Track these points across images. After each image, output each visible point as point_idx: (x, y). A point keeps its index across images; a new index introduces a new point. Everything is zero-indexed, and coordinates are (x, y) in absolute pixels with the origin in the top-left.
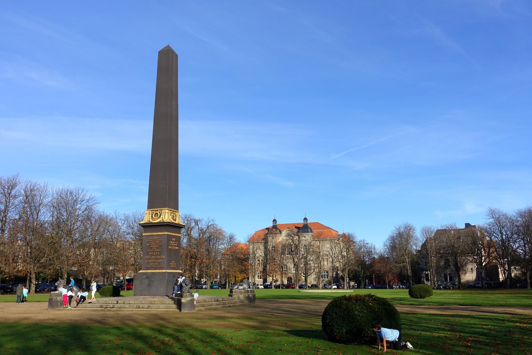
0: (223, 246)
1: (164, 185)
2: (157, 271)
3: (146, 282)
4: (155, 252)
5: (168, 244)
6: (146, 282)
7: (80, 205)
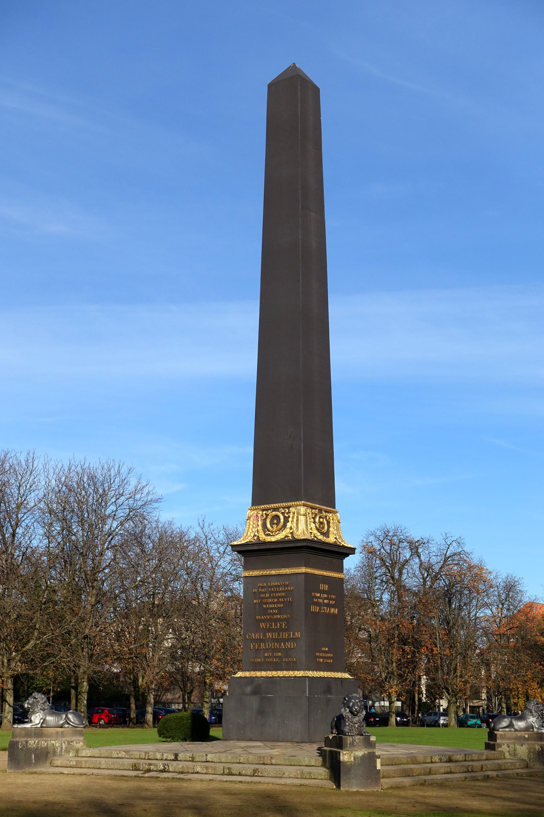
0: (488, 612)
1: (293, 443)
2: (281, 674)
3: (254, 702)
4: (276, 621)
5: (310, 601)
7: (113, 508)
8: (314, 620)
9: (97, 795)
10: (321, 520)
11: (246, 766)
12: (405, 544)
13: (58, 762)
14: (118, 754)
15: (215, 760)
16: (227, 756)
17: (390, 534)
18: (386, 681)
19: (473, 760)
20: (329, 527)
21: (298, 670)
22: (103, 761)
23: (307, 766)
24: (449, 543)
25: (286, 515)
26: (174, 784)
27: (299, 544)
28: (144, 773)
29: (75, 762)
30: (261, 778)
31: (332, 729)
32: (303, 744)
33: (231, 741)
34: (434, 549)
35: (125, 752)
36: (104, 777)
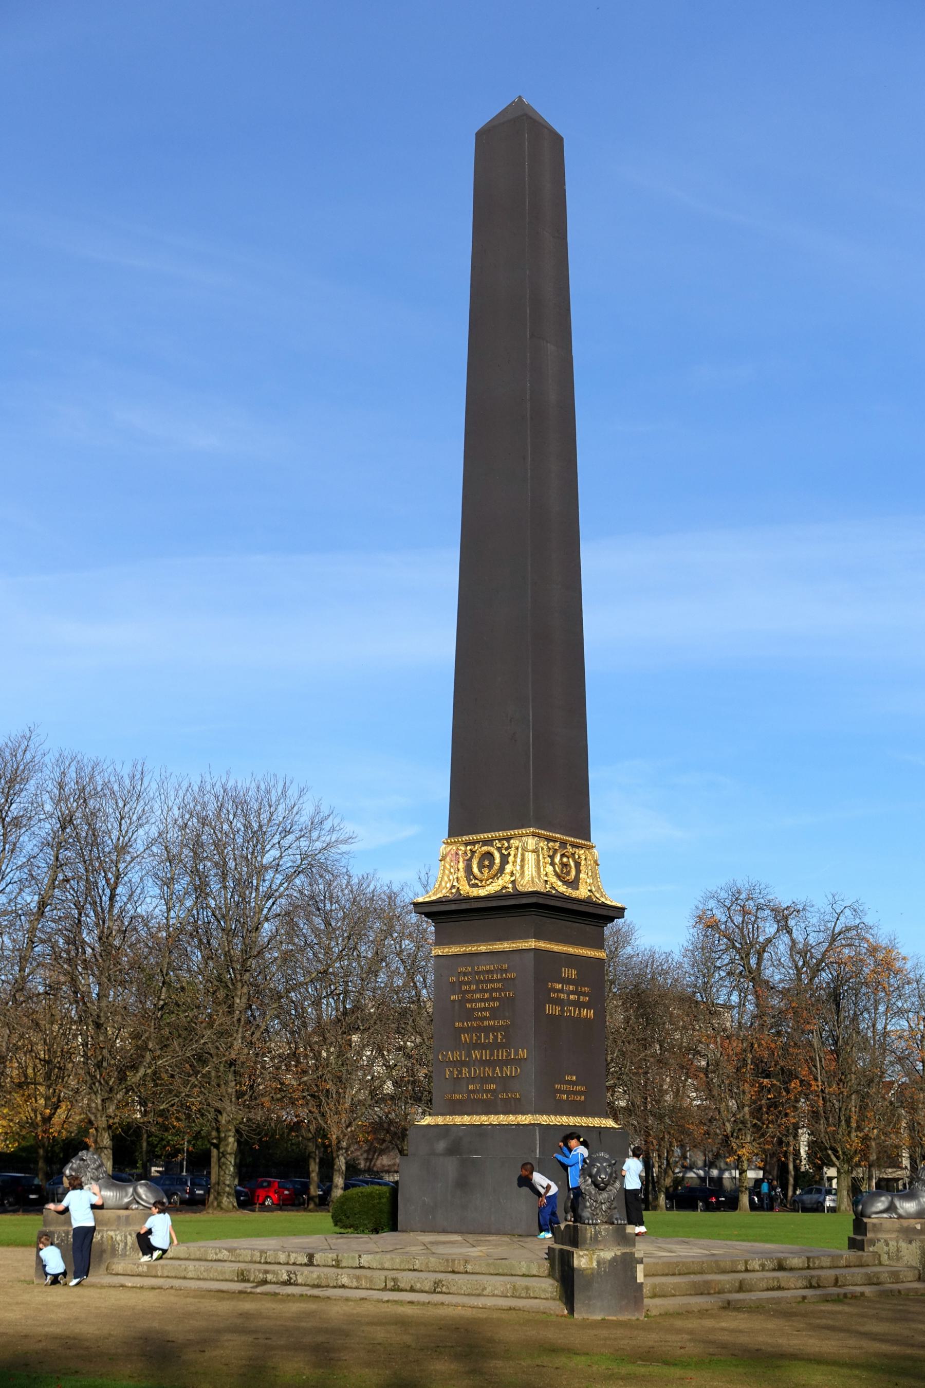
1: (520, 733)
2: (494, 1119)
3: (450, 1166)
5: (543, 996)
6: (450, 1166)
7: (275, 853)
8: (551, 1030)
9: (156, 1325)
10: (565, 860)
11: (422, 1275)
12: (767, 912)
13: (119, 1267)
14: (216, 1254)
15: (374, 1265)
16: (392, 1259)
17: (741, 897)
18: (732, 1136)
19: (822, 1268)
20: (578, 872)
21: (523, 1114)
22: (191, 1265)
23: (524, 1275)
24: (838, 911)
25: (503, 851)
26: (312, 1306)
27: (524, 901)
28: (256, 1287)
29: (145, 1267)
30: (446, 1296)
31: (566, 1213)
32: (529, 1239)
33: (411, 1234)
34: (814, 921)
35: (230, 1250)
36: (188, 1293)
